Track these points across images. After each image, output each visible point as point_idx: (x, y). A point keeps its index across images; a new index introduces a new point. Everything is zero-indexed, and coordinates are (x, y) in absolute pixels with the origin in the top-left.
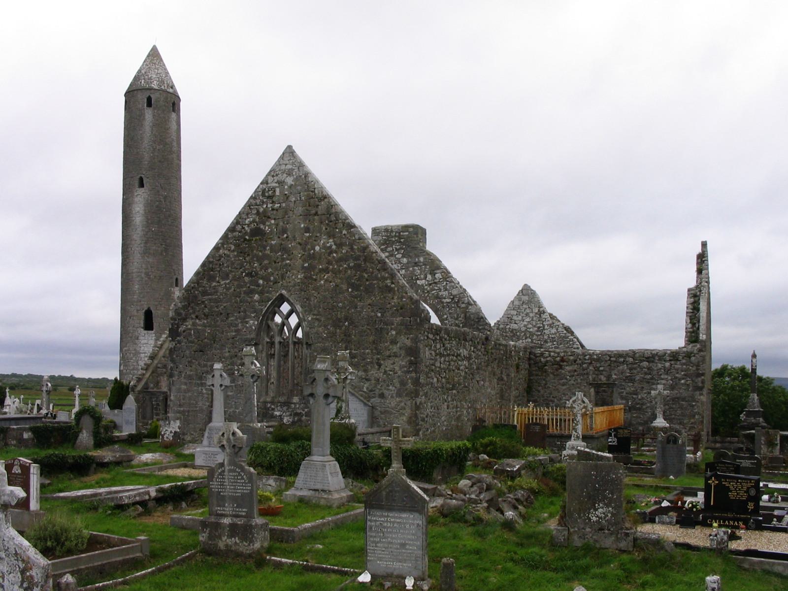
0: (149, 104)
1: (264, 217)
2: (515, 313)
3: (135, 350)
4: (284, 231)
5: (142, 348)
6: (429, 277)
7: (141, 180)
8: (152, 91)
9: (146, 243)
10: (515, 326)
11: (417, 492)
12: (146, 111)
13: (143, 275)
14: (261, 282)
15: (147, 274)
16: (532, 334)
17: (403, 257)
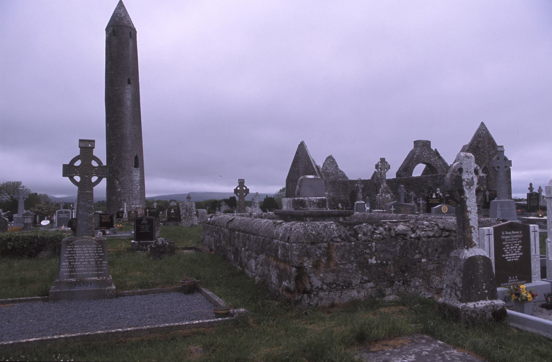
0: (131, 37)
1: (479, 142)
2: (328, 166)
3: (130, 179)
4: (484, 147)
5: (134, 178)
6: (434, 158)
7: (129, 80)
9: (133, 117)
10: (328, 171)
11: (534, 219)
12: (130, 40)
13: (133, 136)
14: (479, 162)
16: (334, 174)
17: (427, 151)
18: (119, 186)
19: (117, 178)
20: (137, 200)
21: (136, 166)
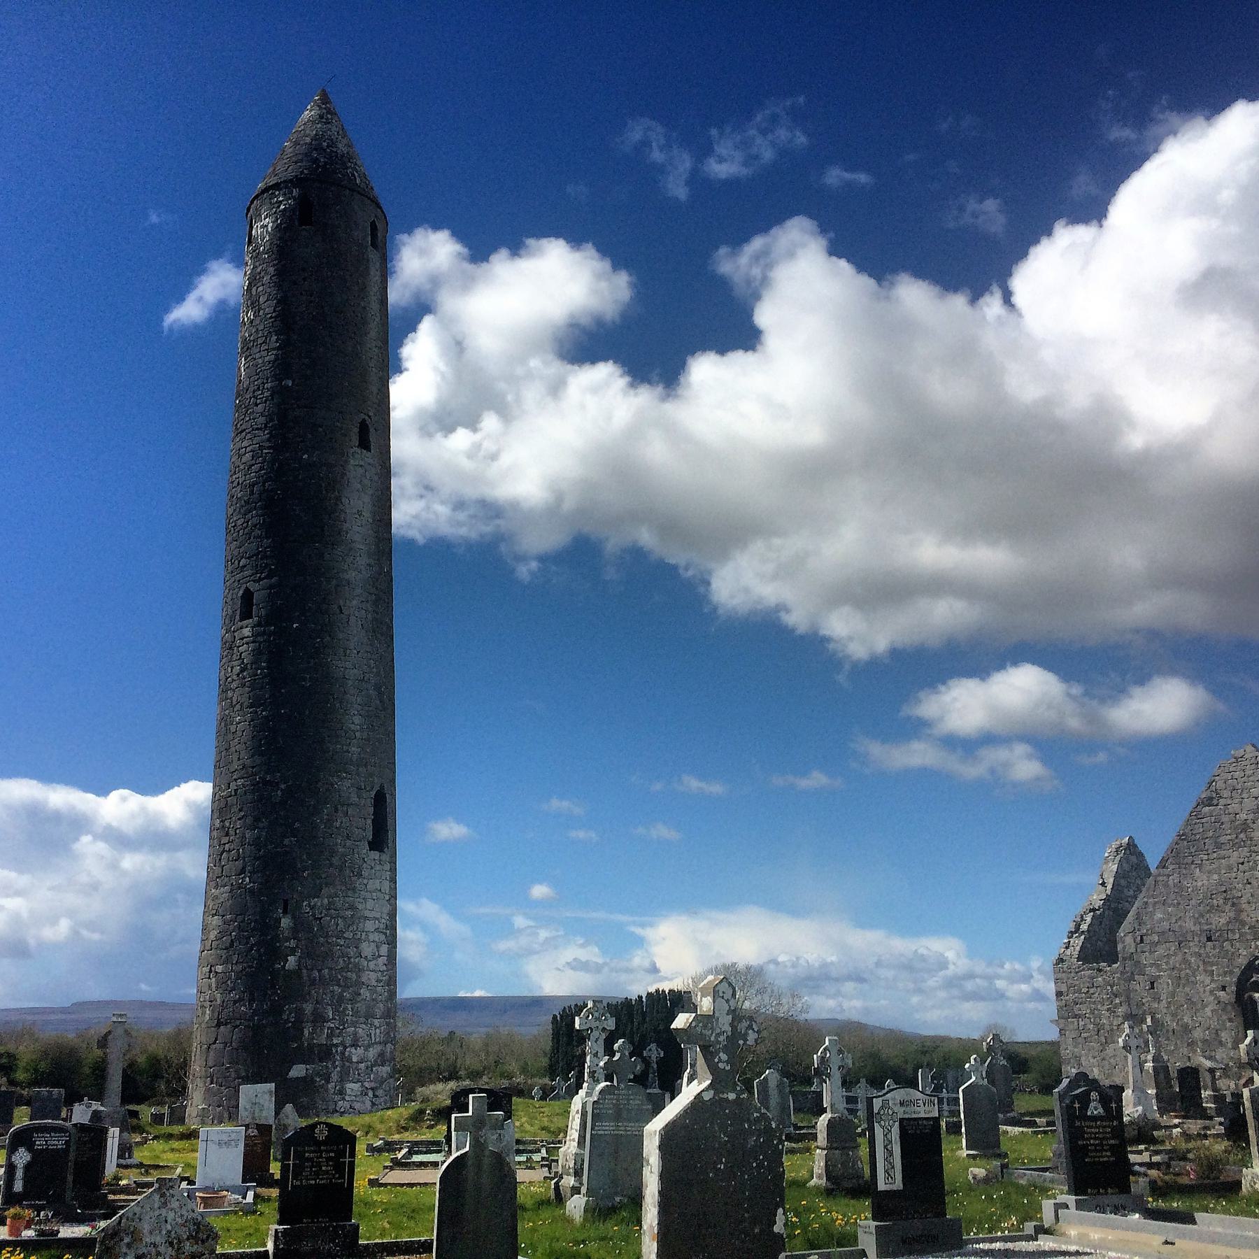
18: (293, 943)
19: (286, 903)
20: (376, 1022)
21: (364, 444)
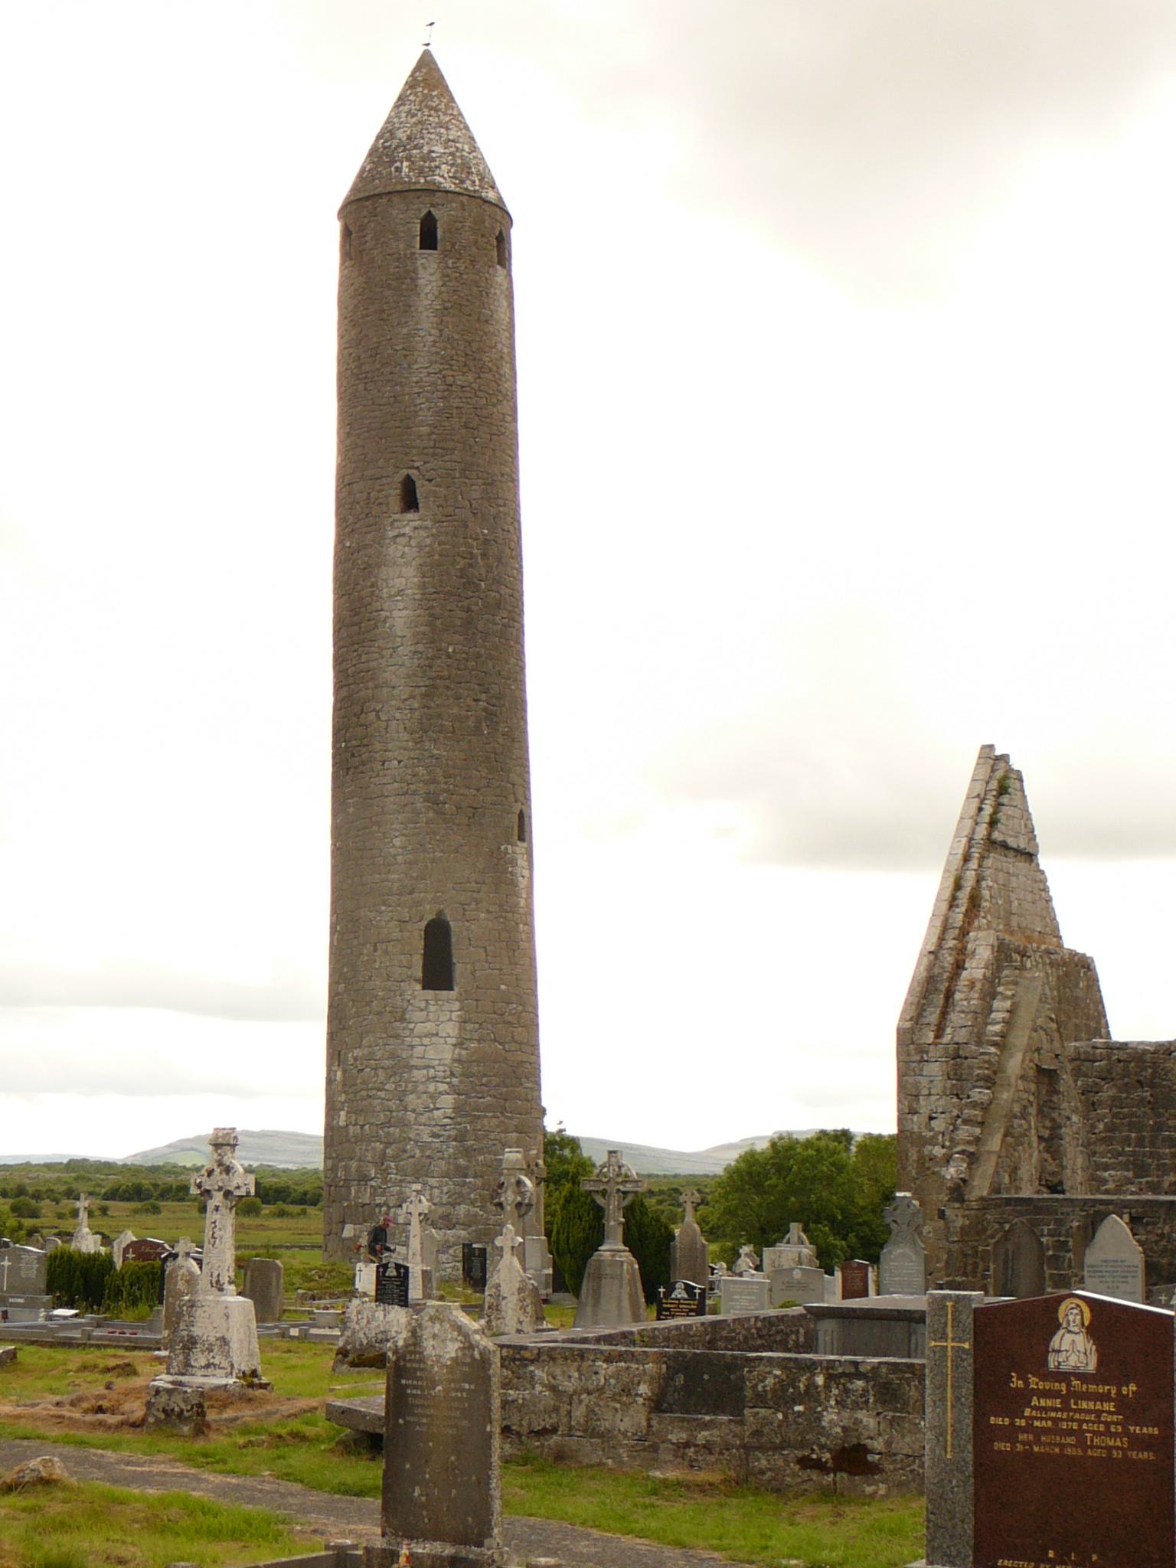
8: (438, 198)
15: (433, 800)
